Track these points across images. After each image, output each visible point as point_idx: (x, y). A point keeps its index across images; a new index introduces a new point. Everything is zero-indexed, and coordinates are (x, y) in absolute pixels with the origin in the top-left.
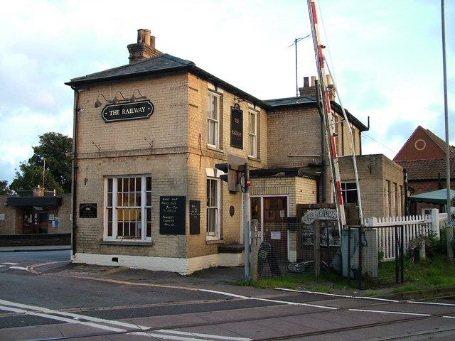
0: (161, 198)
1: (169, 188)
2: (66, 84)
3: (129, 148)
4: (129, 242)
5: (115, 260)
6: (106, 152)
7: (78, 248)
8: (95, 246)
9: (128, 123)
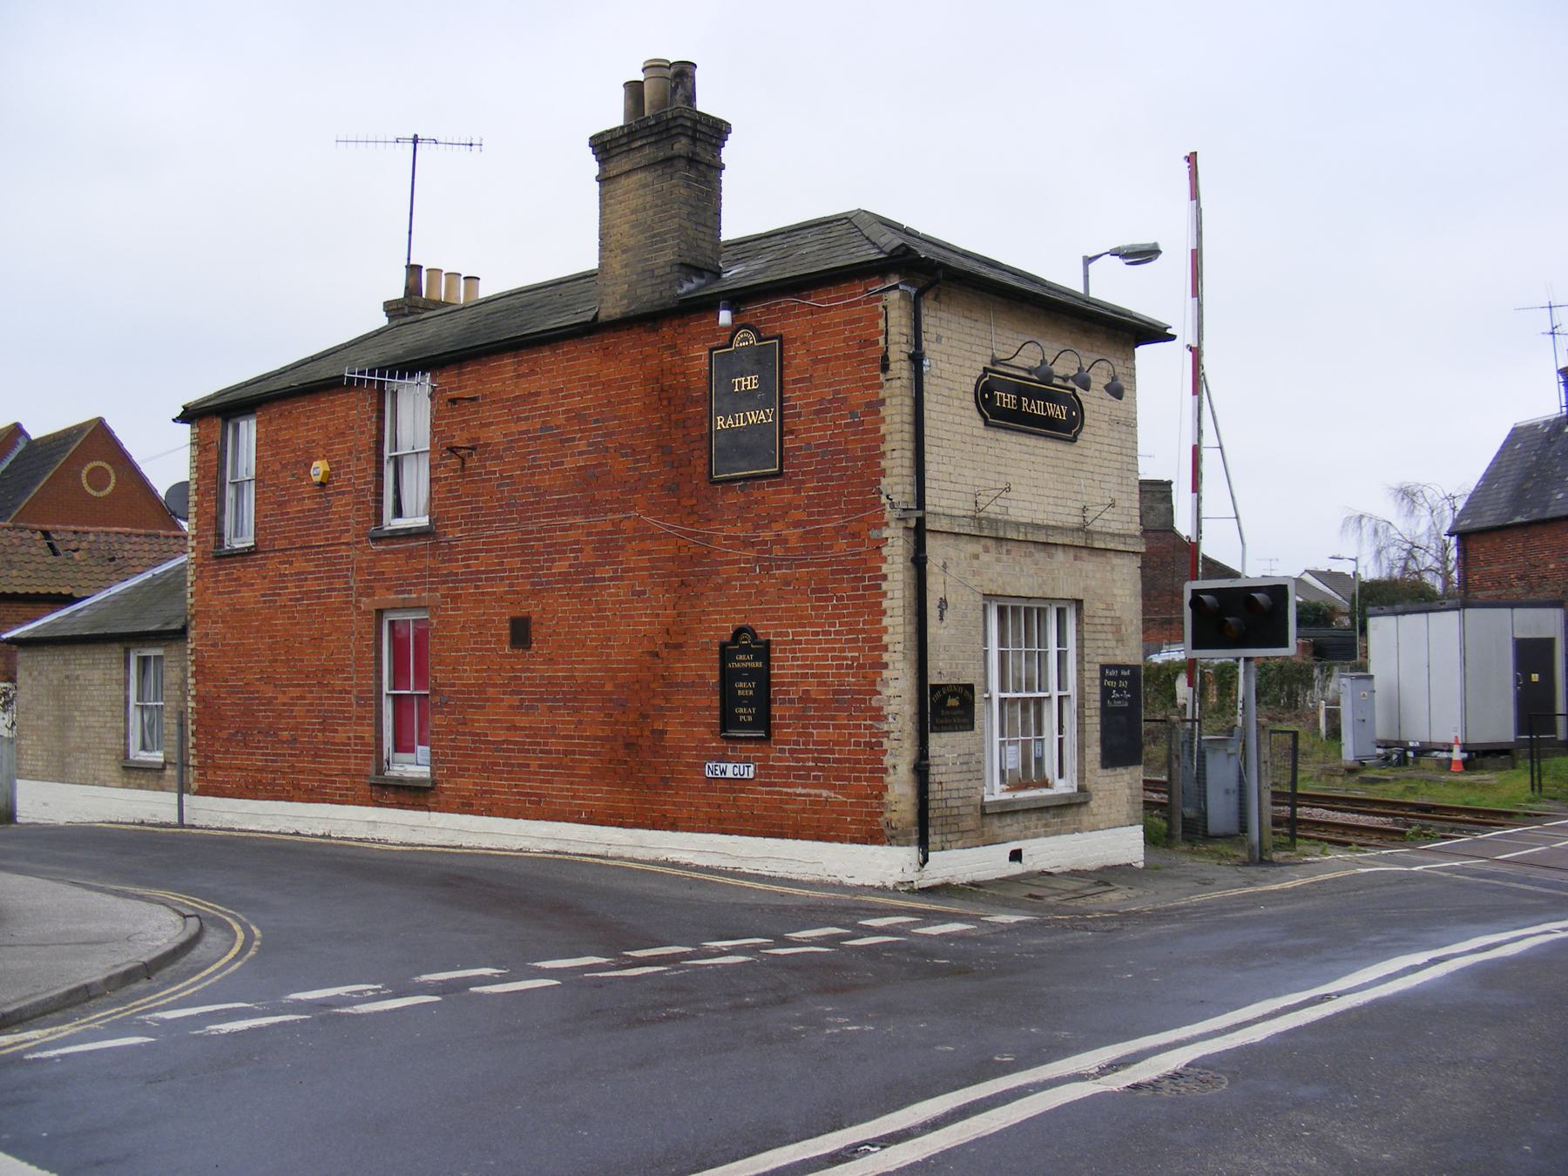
0: (1103, 667)
1: (1113, 644)
2: (174, 420)
3: (1040, 518)
4: (1035, 799)
5: (1016, 856)
6: (993, 522)
7: (934, 839)
8: (969, 823)
9: (1031, 441)
